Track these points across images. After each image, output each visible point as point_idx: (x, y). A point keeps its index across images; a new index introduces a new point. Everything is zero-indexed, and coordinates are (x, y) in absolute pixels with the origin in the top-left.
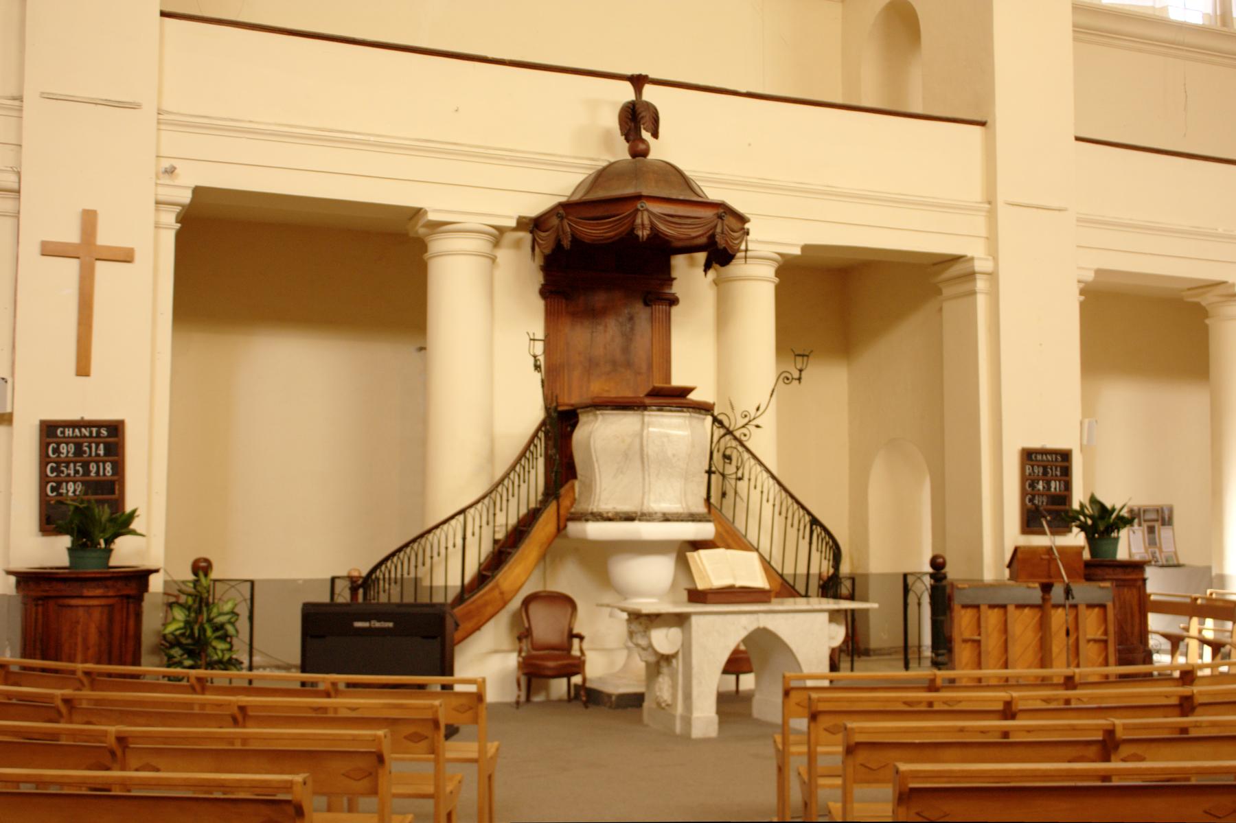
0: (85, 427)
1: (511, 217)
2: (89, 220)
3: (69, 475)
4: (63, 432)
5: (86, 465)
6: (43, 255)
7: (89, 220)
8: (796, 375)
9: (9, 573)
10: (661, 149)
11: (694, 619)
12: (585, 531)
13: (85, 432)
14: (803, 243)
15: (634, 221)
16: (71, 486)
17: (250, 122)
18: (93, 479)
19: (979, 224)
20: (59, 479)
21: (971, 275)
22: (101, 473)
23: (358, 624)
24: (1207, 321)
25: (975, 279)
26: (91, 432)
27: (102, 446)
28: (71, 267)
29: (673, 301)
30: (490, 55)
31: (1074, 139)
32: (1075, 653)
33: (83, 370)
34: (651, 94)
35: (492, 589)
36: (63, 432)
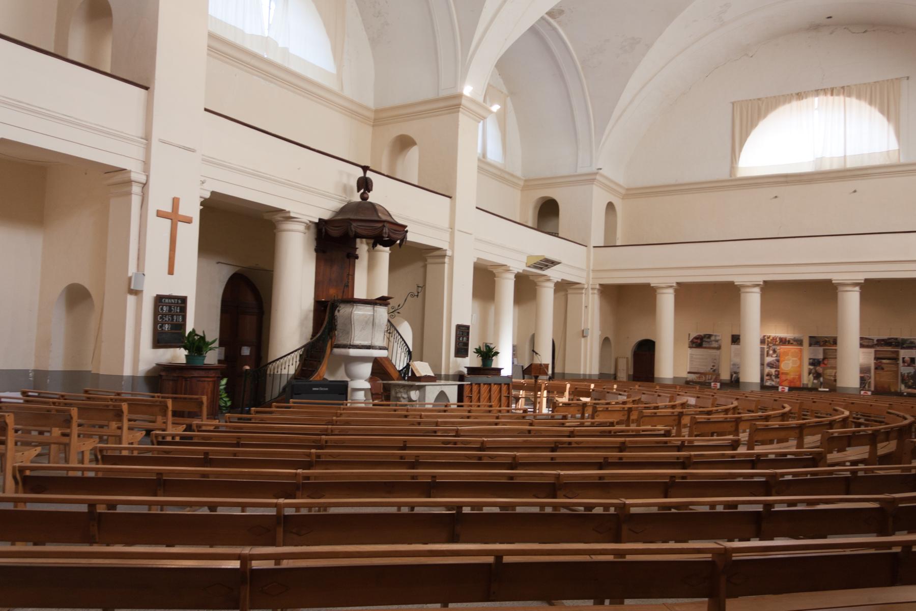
0: (173, 299)
1: (316, 218)
2: (176, 202)
3: (166, 321)
4: (165, 301)
5: (172, 316)
6: (157, 216)
7: (176, 202)
8: (416, 294)
9: (465, 367)
10: (373, 197)
11: (427, 387)
12: (348, 353)
13: (173, 301)
14: (211, 190)
15: (383, 230)
16: (167, 326)
17: (230, 163)
18: (179, 323)
19: (447, 236)
20: (163, 322)
21: (129, 182)
22: (178, 320)
23: (314, 389)
24: (496, 279)
25: (445, 258)
26: (175, 301)
27: (178, 308)
28: (168, 222)
29: (357, 257)
30: (312, 147)
31: (203, 109)
32: (479, 400)
33: (171, 272)
34: (369, 174)
35: (317, 376)
36: (165, 301)
